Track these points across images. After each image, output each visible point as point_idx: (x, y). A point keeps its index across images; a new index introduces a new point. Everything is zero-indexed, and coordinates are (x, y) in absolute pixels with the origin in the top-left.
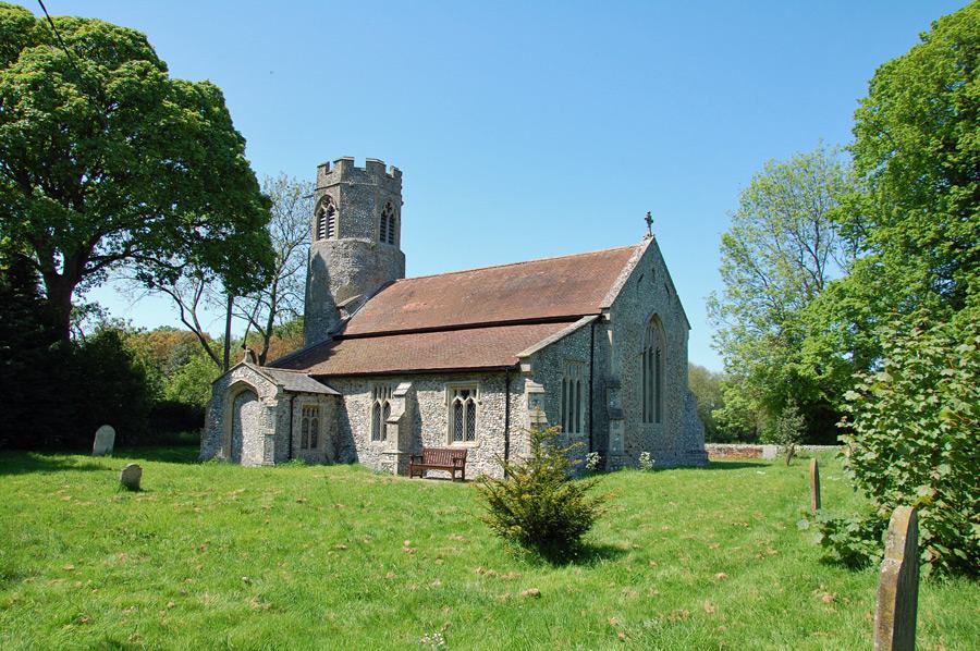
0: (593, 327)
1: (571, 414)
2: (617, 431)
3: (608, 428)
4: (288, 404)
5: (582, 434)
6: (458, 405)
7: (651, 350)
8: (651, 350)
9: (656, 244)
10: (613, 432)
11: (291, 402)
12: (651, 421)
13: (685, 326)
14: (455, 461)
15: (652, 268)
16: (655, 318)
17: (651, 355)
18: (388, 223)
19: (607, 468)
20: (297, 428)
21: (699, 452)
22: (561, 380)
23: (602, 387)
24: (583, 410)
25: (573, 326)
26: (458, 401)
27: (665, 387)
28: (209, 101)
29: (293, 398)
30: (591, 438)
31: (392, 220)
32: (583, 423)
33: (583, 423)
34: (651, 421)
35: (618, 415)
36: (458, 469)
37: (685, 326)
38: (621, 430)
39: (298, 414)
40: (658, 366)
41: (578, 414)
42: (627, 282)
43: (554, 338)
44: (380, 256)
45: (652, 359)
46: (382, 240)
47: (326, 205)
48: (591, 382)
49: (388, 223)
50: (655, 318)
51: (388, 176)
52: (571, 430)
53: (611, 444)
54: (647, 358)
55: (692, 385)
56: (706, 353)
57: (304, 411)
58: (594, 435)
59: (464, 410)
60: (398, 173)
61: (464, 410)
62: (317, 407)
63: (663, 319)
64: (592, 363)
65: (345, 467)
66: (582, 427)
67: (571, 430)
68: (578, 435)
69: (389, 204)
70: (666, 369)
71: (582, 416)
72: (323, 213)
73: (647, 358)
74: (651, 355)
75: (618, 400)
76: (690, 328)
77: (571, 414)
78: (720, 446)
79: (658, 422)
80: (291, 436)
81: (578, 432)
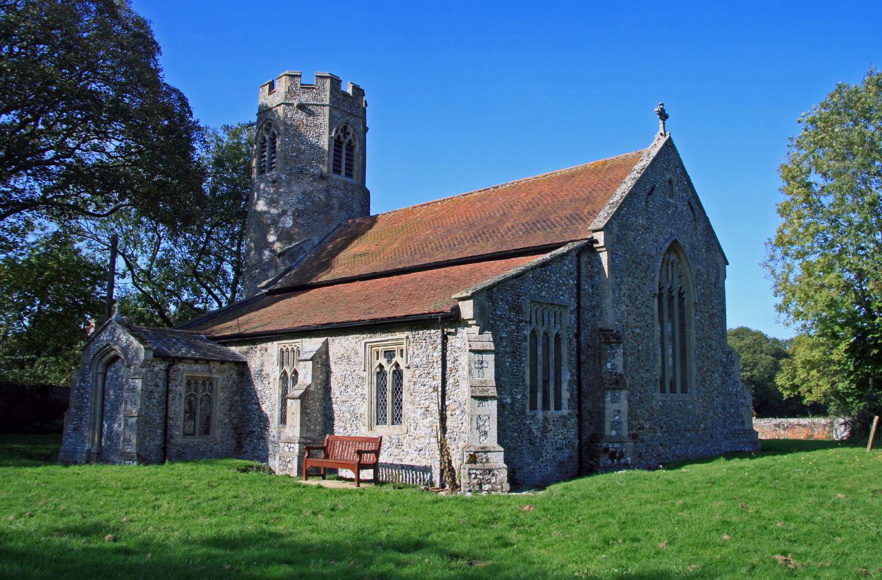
0: (578, 256)
1: (546, 382)
2: (616, 406)
3: (604, 402)
4: (162, 375)
5: (565, 411)
6: (381, 372)
7: (670, 291)
8: (670, 291)
9: (673, 146)
10: (610, 407)
11: (167, 371)
12: (673, 391)
13: (720, 260)
14: (360, 453)
15: (667, 184)
16: (674, 247)
17: (671, 298)
18: (344, 152)
19: (604, 460)
20: (178, 407)
21: (745, 431)
22: (527, 332)
23: (593, 343)
24: (566, 377)
25: (547, 256)
26: (381, 366)
27: (693, 343)
28: (141, 23)
29: (169, 367)
30: (579, 416)
31: (350, 148)
32: (566, 395)
33: (566, 395)
34: (673, 391)
35: (617, 383)
36: (367, 466)
37: (720, 260)
38: (623, 405)
39: (179, 389)
40: (682, 315)
41: (393, 340)
42: (630, 193)
43: (513, 272)
44: (333, 191)
45: (671, 301)
46: (337, 170)
47: (267, 130)
48: (577, 336)
49: (344, 152)
50: (674, 247)
51: (346, 95)
52: (546, 406)
53: (608, 425)
54: (665, 303)
55: (731, 342)
56: (757, 304)
57: (189, 384)
58: (585, 415)
59: (390, 378)
60: (358, 91)
61: (390, 378)
62: (209, 379)
63: (687, 248)
64: (579, 308)
65: (224, 470)
66: (565, 402)
67: (546, 406)
68: (559, 413)
69: (345, 128)
70: (693, 317)
71: (565, 386)
72: (265, 141)
73: (665, 303)
74: (671, 298)
75: (619, 361)
76: (728, 264)
77: (546, 382)
78: (778, 421)
79: (684, 391)
80: (166, 418)
81: (558, 407)
